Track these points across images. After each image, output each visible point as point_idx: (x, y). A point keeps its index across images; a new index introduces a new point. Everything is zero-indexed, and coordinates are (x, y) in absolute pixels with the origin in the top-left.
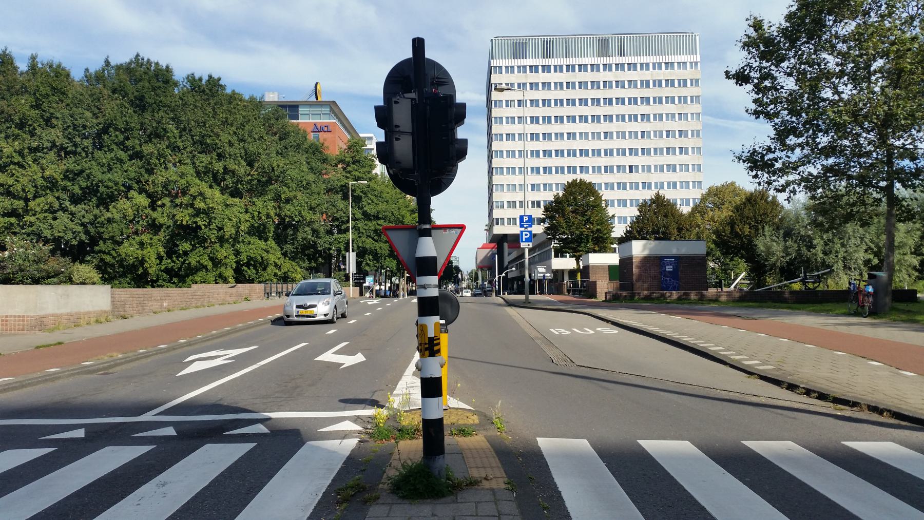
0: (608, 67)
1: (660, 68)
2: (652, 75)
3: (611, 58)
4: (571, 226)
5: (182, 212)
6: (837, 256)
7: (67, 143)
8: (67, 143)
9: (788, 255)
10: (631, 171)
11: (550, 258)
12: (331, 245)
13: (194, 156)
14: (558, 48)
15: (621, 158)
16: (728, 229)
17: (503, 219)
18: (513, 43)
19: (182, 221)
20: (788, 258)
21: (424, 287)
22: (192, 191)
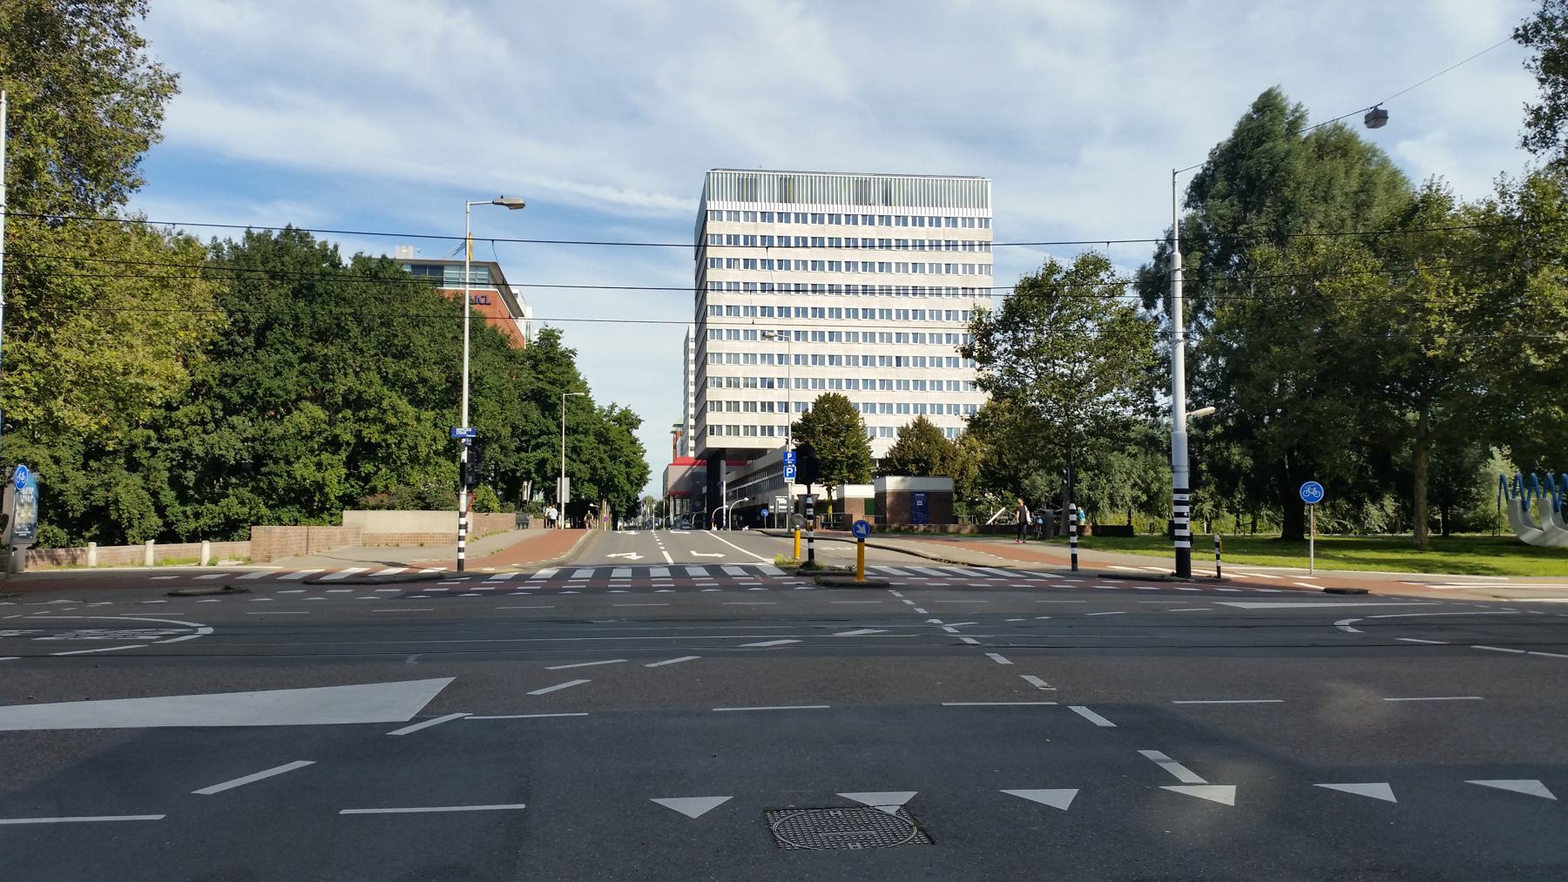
0: (868, 219)
1: (938, 225)
2: (928, 232)
3: (873, 207)
4: (822, 449)
5: (369, 427)
6: (1103, 493)
7: (222, 341)
8: (222, 341)
9: (1052, 489)
10: (899, 364)
12: (517, 466)
13: (379, 360)
14: (801, 190)
16: (996, 458)
17: (720, 427)
18: (739, 179)
19: (370, 438)
20: (1053, 493)
22: (385, 404)
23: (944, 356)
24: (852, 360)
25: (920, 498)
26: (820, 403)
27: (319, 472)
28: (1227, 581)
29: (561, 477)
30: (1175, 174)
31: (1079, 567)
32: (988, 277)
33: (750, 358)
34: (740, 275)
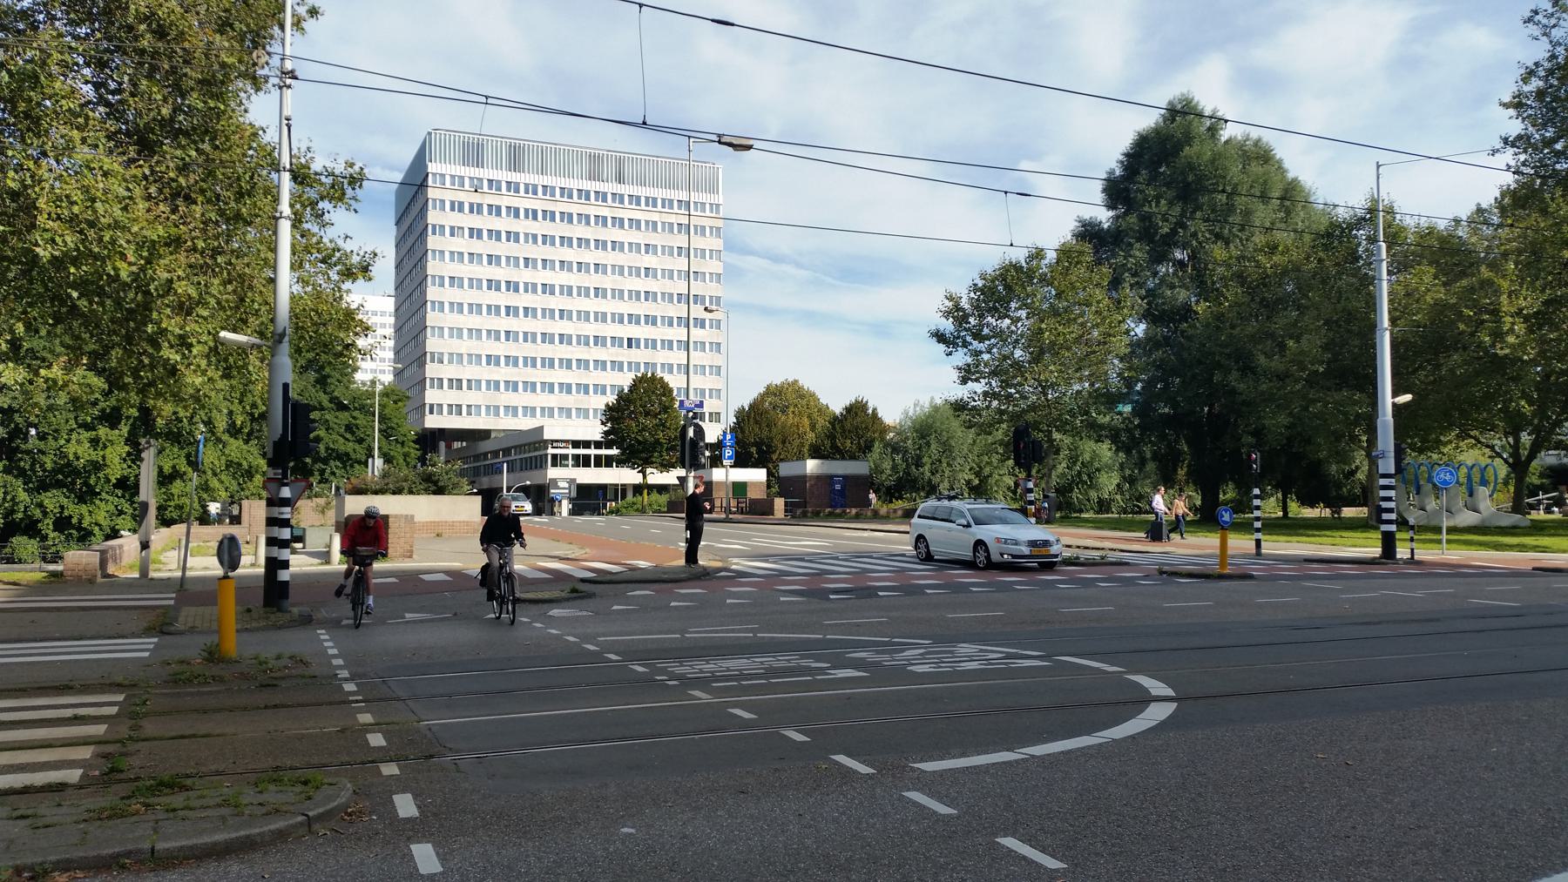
0: (601, 196)
10: (630, 346)
11: (546, 468)
15: (617, 326)
16: (828, 443)
17: (440, 406)
21: (282, 513)
23: (675, 339)
24: (584, 341)
25: (839, 482)
26: (637, 383)
27: (95, 450)
28: (1420, 563)
29: (373, 457)
30: (1378, 166)
31: (1263, 551)
32: (718, 262)
33: (475, 333)
34: (463, 244)
